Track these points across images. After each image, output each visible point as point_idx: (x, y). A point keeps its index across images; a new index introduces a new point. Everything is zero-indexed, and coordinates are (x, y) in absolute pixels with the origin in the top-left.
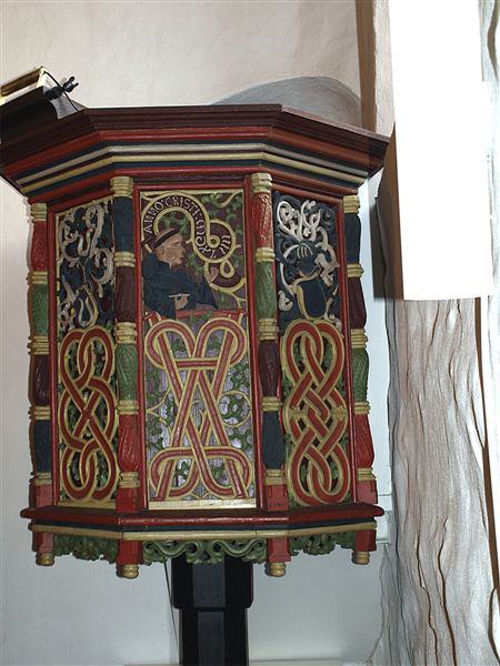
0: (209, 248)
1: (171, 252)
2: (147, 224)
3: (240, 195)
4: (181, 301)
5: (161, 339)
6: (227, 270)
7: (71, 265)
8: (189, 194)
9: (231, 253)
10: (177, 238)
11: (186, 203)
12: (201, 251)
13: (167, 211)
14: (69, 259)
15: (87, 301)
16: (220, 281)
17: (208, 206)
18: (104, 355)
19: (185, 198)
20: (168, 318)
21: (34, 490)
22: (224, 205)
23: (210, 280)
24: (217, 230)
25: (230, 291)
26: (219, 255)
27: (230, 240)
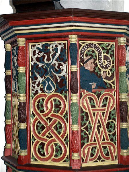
0: (103, 65)
1: (89, 66)
2: (81, 54)
3: (113, 44)
4: (94, 85)
5: (86, 100)
6: (109, 73)
7: (40, 66)
8: (96, 43)
9: (110, 67)
10: (92, 60)
11: (95, 46)
12: (100, 66)
13: (88, 50)
14: (38, 63)
15: (50, 82)
16: (107, 78)
17: (103, 48)
18: (61, 105)
19: (95, 44)
20: (89, 92)
21: (5, 149)
22: (108, 48)
23: (103, 76)
24: (106, 58)
25: (110, 82)
26: (106, 68)
27: (110, 62)
